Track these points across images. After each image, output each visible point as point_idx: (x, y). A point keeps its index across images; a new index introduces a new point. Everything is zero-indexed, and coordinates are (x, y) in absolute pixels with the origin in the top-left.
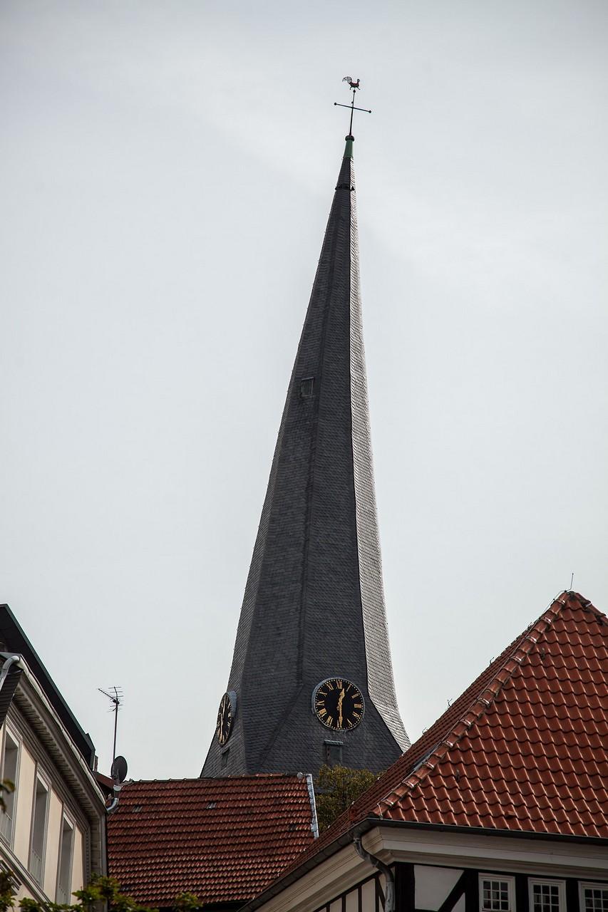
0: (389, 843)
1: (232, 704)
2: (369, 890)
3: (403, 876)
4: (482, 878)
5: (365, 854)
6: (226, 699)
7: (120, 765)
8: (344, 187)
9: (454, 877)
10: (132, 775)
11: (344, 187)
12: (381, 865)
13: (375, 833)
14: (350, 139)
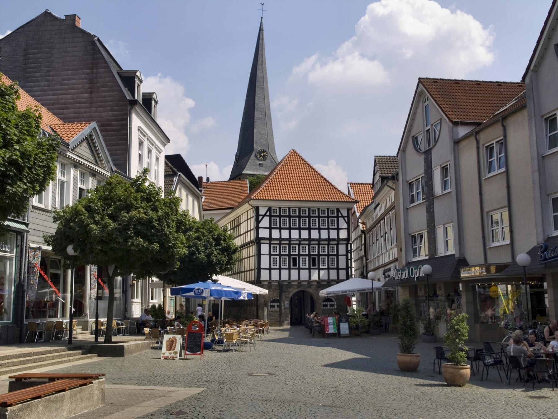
0: (252, 202)
1: (238, 155)
2: (252, 210)
3: (257, 209)
4: (272, 208)
5: (250, 205)
6: (237, 153)
7: (208, 179)
8: (261, 30)
9: (267, 208)
10: (211, 180)
11: (261, 30)
12: (253, 207)
13: (251, 201)
14: (262, 18)
